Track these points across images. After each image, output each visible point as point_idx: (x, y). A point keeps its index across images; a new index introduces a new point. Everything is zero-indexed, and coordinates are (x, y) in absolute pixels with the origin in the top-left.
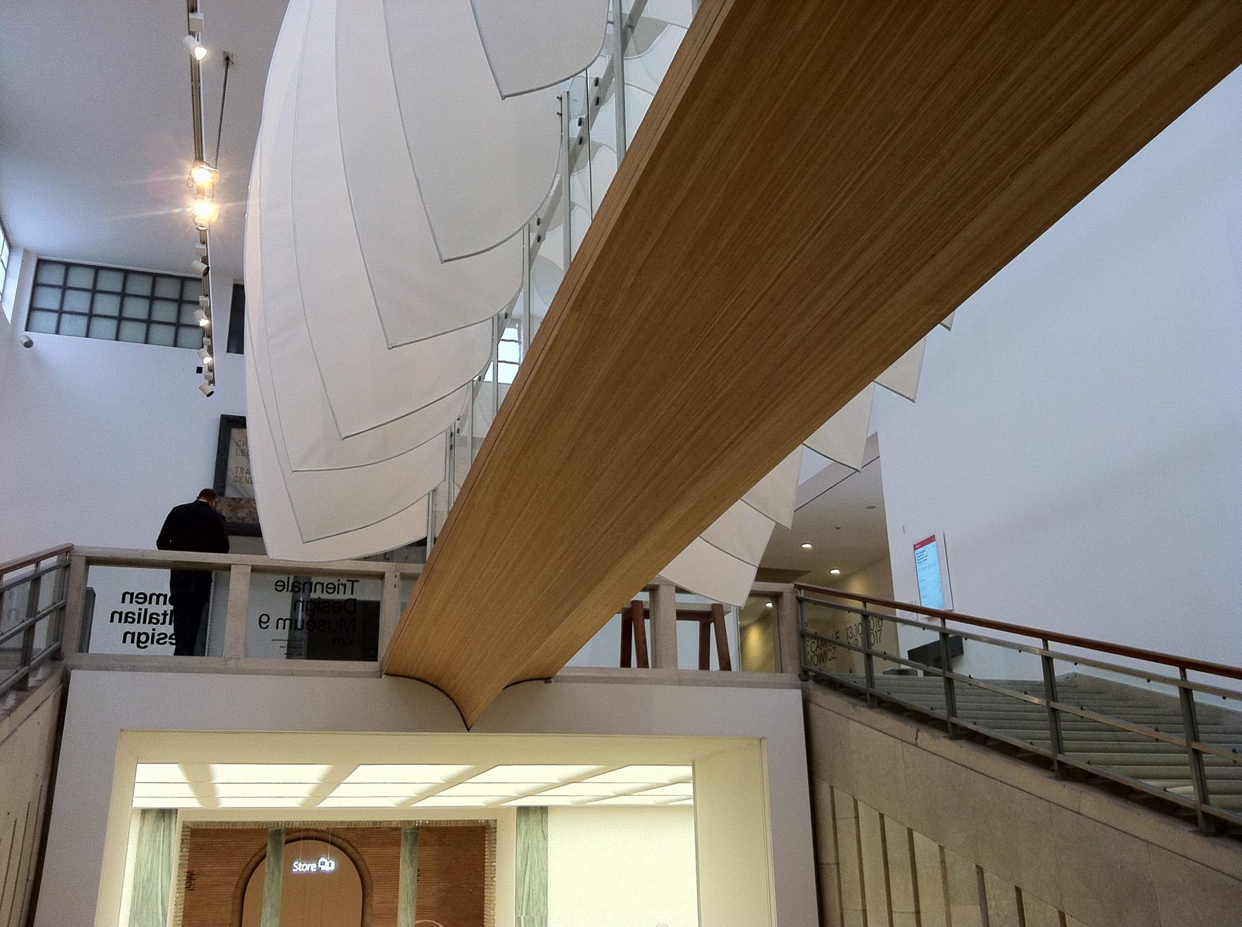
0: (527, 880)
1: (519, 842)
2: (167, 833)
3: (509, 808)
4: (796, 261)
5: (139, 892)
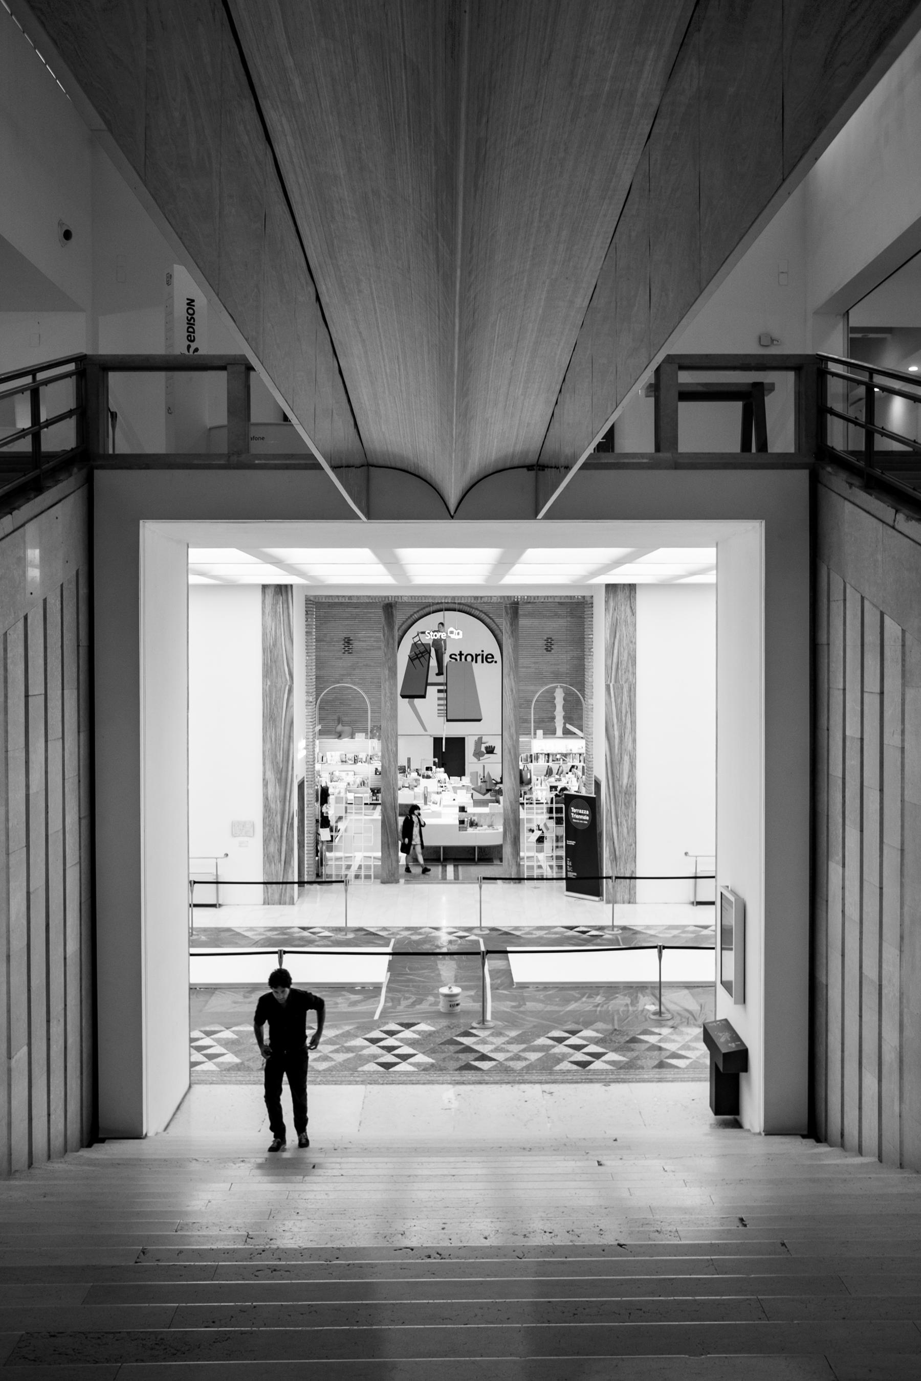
0: (616, 651)
1: (607, 617)
2: (285, 606)
3: (599, 585)
4: (405, 19)
5: (267, 656)
